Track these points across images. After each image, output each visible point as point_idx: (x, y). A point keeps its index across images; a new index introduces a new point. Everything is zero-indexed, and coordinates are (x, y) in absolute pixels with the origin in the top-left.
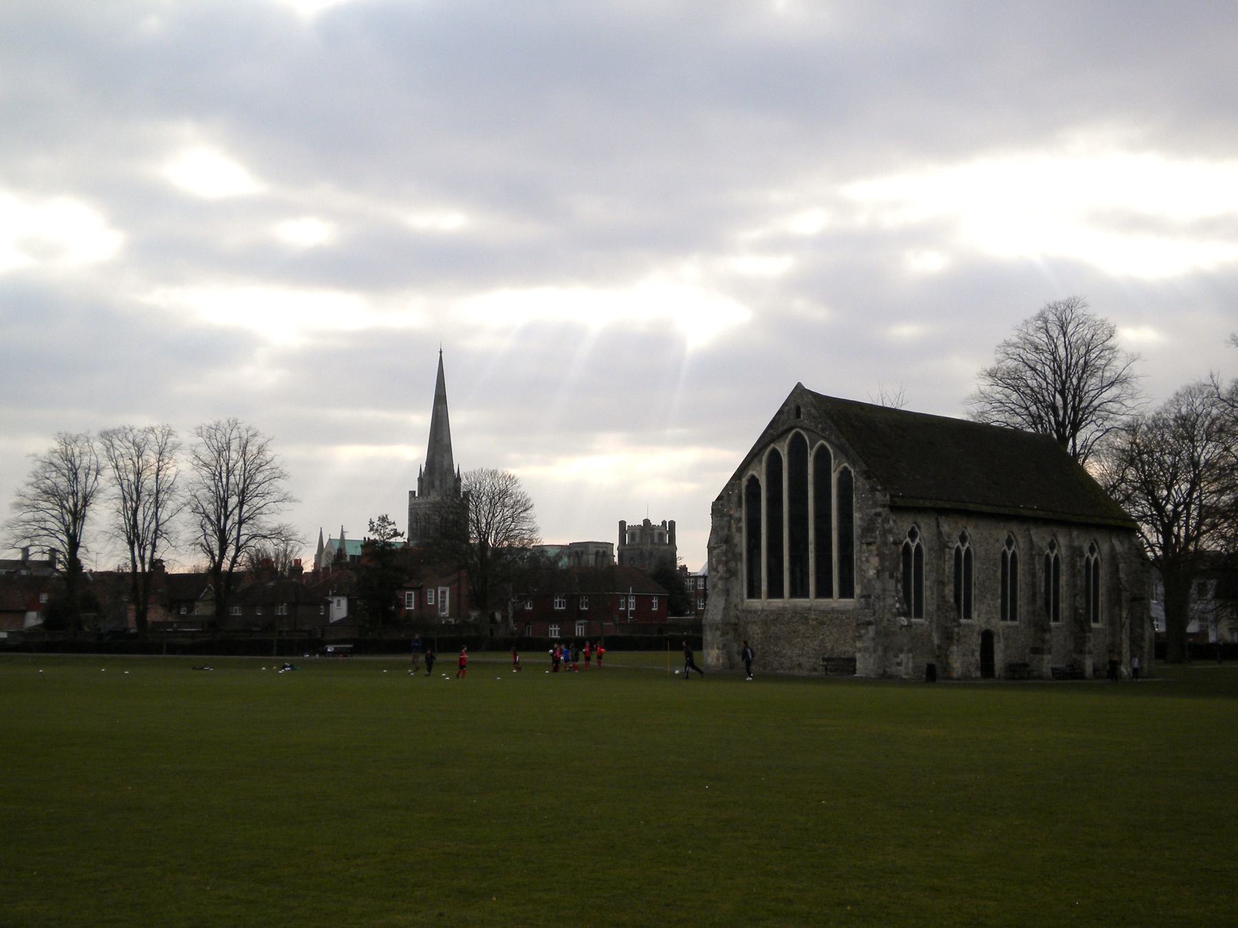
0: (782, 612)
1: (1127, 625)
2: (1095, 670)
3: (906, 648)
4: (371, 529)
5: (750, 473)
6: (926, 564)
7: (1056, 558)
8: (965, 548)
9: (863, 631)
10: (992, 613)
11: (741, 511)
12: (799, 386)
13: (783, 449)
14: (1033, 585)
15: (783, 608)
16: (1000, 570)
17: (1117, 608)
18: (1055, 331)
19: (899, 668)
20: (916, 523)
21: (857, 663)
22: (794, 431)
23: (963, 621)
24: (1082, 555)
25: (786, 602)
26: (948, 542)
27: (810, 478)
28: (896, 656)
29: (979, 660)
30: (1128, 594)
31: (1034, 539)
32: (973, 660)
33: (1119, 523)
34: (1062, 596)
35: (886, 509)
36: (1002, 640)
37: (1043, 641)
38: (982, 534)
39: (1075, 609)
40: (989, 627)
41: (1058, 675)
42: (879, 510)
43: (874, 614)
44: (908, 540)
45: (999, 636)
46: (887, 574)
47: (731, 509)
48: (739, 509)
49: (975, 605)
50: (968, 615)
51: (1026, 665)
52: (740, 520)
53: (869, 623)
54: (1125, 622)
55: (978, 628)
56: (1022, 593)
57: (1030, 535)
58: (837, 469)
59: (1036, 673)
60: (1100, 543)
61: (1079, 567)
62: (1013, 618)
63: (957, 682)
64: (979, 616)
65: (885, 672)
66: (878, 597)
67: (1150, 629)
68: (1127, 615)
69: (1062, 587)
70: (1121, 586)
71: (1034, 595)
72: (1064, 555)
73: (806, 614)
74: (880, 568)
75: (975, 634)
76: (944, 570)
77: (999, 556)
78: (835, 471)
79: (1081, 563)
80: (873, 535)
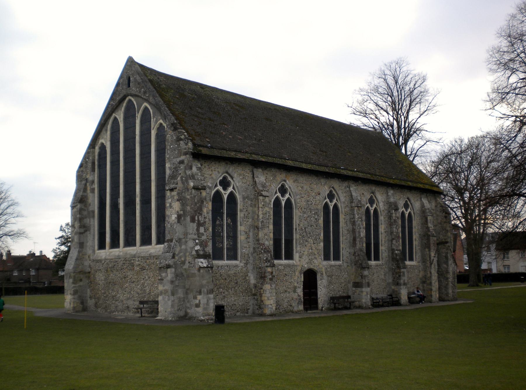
0: (117, 260)
1: (435, 262)
2: (409, 298)
3: (205, 290)
4: (61, 230)
6: (241, 211)
7: (376, 210)
9: (164, 275)
10: (315, 255)
11: (94, 174)
12: (131, 62)
13: (120, 115)
15: (119, 256)
16: (322, 218)
17: (427, 250)
18: (391, 82)
19: (197, 309)
20: (227, 173)
21: (159, 305)
22: (127, 99)
24: (397, 209)
25: (122, 251)
28: (195, 298)
29: (302, 295)
30: (435, 239)
31: (354, 194)
32: (295, 296)
33: (427, 187)
34: (382, 240)
37: (362, 277)
38: (302, 187)
40: (312, 267)
41: (376, 303)
42: (183, 158)
43: (173, 257)
46: (188, 219)
47: (87, 174)
48: (92, 173)
49: (296, 248)
50: (289, 256)
51: (349, 297)
52: (93, 182)
53: (168, 266)
54: (433, 260)
55: (299, 268)
57: (350, 191)
58: (154, 126)
59: (357, 304)
60: (412, 201)
61: (394, 218)
62: (337, 257)
63: (270, 319)
64: (300, 257)
65: (186, 314)
66: (179, 241)
67: (453, 265)
68: (435, 254)
69: (382, 234)
70: (429, 233)
71: (354, 239)
73: (132, 261)
74: (182, 212)
75: (297, 273)
76: (258, 216)
77: (321, 207)
79: (396, 215)
80: (175, 181)
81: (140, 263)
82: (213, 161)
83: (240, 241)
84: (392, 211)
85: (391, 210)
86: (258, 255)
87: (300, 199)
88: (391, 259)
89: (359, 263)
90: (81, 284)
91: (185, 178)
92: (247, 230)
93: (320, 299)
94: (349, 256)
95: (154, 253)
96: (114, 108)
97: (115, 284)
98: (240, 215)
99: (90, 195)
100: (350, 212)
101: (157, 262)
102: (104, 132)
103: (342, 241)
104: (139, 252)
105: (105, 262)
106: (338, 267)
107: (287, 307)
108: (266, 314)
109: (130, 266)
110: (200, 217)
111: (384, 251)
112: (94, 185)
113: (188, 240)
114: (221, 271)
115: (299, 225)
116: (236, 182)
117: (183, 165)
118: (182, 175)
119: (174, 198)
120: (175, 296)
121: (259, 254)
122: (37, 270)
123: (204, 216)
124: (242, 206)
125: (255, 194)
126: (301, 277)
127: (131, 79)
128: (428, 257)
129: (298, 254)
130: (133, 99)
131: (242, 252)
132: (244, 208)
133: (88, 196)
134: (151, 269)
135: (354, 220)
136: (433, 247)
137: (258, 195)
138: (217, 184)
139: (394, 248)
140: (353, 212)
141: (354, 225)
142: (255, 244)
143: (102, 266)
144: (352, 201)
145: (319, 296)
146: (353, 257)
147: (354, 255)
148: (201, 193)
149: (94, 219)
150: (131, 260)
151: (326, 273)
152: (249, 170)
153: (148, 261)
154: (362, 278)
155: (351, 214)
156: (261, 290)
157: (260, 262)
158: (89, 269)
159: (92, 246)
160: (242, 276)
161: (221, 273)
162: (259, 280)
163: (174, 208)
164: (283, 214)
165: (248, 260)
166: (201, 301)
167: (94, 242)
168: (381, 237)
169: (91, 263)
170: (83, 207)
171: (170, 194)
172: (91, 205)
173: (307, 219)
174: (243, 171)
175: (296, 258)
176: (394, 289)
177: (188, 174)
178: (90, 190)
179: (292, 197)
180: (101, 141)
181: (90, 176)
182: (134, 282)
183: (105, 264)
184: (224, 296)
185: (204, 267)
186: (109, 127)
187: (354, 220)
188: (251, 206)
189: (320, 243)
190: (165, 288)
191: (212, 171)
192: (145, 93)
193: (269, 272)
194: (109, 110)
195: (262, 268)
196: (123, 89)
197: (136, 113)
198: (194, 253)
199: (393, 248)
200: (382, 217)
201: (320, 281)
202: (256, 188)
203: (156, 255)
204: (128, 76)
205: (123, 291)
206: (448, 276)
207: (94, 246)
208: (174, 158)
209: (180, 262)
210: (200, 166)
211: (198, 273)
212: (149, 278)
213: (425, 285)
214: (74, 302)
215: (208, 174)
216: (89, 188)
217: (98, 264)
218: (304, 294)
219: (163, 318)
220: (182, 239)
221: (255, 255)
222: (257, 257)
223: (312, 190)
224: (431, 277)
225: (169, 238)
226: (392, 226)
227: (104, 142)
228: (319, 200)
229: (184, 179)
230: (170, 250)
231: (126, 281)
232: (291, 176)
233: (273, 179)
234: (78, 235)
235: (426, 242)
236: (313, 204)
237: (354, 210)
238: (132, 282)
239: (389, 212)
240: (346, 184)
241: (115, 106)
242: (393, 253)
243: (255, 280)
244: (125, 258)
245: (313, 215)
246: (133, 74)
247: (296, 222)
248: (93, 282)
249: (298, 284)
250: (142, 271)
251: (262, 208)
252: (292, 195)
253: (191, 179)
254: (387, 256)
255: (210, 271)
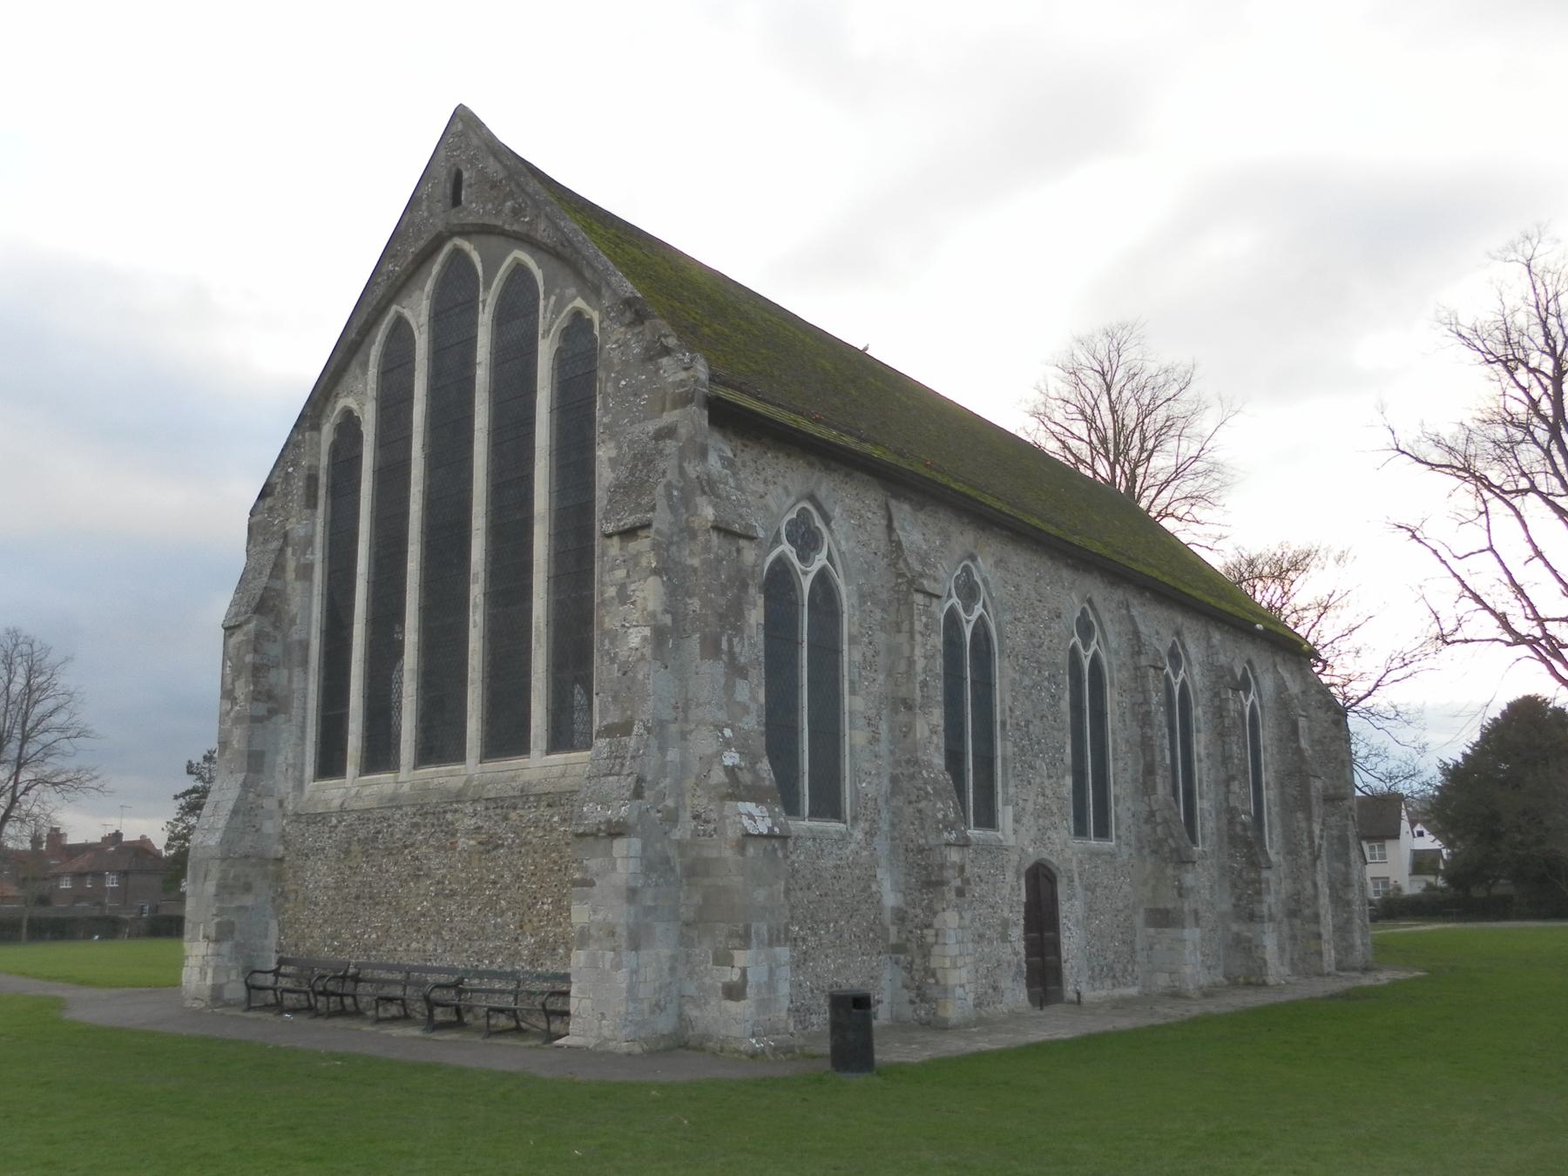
0: (388, 813)
5: (343, 403)
6: (853, 640)
8: (974, 618)
9: (593, 864)
10: (1053, 814)
13: (417, 310)
14: (1146, 744)
17: (1300, 815)
19: (732, 1006)
20: (812, 498)
23: (973, 833)
26: (921, 575)
27: (482, 375)
28: (724, 959)
29: (1023, 952)
31: (1142, 628)
35: (693, 408)
36: (1079, 890)
37: (1182, 892)
38: (1017, 587)
39: (1232, 813)
40: (1045, 855)
44: (786, 548)
45: (1071, 880)
46: (694, 643)
49: (1005, 785)
50: (987, 818)
52: (309, 542)
53: (616, 831)
54: (1320, 845)
56: (1121, 764)
58: (551, 326)
60: (1258, 671)
62: (1102, 831)
64: (1017, 820)
69: (1200, 761)
71: (1149, 770)
72: (1199, 685)
73: (449, 816)
75: (1010, 876)
76: (911, 662)
77: (1063, 658)
78: (547, 332)
80: (645, 500)
81: (480, 824)
82: (769, 449)
83: (851, 750)
84: (1227, 693)
85: (1222, 691)
86: (910, 802)
87: (1011, 623)
88: (1226, 839)
89: (1166, 849)
90: (248, 900)
91: (681, 490)
92: (872, 713)
93: (1068, 965)
94: (1134, 824)
95: (539, 782)
96: (398, 283)
97: (377, 904)
98: (850, 656)
99: (294, 587)
100: (1133, 685)
101: (552, 816)
102: (358, 371)
103: (1114, 775)
104: (475, 783)
105: (340, 822)
106: (1107, 858)
107: (986, 993)
108: (946, 1020)
109: (441, 835)
110: (736, 640)
111: (1207, 815)
112: (312, 553)
113: (693, 726)
114: (793, 857)
115: (1011, 710)
116: (838, 536)
117: (674, 443)
118: (669, 476)
119: (636, 564)
120: (642, 952)
121: (914, 798)
122: (124, 874)
123: (750, 637)
124: (857, 623)
125: (898, 585)
126: (1020, 889)
127: (466, 175)
128: (1305, 838)
129: (1010, 809)
130: (467, 246)
131: (857, 792)
132: (864, 631)
133: (289, 590)
134: (525, 844)
135: (1145, 708)
136: (1317, 810)
137: (908, 589)
138: (778, 533)
139: (1237, 805)
140: (1143, 686)
141: (1145, 724)
142: (897, 763)
143: (329, 838)
144: (1137, 649)
145: (1064, 955)
146: (1147, 828)
147: (1147, 821)
148: (739, 551)
149: (306, 672)
150: (445, 812)
151: (1080, 875)
152: (876, 500)
153: (513, 815)
154: (1180, 895)
155: (1136, 689)
156: (925, 931)
157: (923, 829)
158: (281, 848)
159: (294, 766)
160: (859, 878)
161: (793, 862)
162: (917, 894)
163: (639, 601)
164: (968, 669)
165: (874, 821)
166: (749, 977)
167: (303, 753)
168: (1200, 770)
169: (288, 824)
170: (269, 629)
171: (621, 549)
172: (298, 621)
173: (1031, 694)
174: (857, 500)
175: (1004, 822)
176: (1238, 934)
177: (694, 476)
178: (297, 570)
179: (991, 615)
180: (345, 402)
181: (298, 523)
182: (453, 893)
183: (341, 828)
184: (805, 953)
185: (761, 836)
186: (375, 352)
187: (1145, 708)
188: (883, 629)
189: (1063, 777)
190: (600, 917)
191: (765, 482)
192: (517, 213)
193: (954, 865)
194: (379, 291)
195: (930, 849)
196: (431, 215)
197: (481, 289)
198: (718, 776)
199: (1231, 805)
200: (1200, 709)
201: (1068, 905)
202: (901, 564)
203: (550, 788)
204: (454, 169)
205: (411, 930)
206: (1351, 896)
207: (303, 764)
208: (632, 423)
209: (659, 815)
210: (730, 455)
211: (740, 858)
212: (519, 877)
213: (1297, 922)
214: (216, 969)
215: (753, 493)
216: (291, 565)
217: (313, 828)
218: (1027, 948)
219: (591, 1042)
220: (667, 721)
221: (898, 801)
222: (909, 810)
223: (1040, 601)
224: (1316, 897)
225: (616, 721)
226: (1227, 739)
227: (354, 406)
228: (1059, 636)
229: (675, 493)
230: (622, 765)
231: (422, 892)
232: (990, 546)
233: (942, 546)
234: (245, 726)
235: (1295, 793)
236: (1045, 648)
237: (1145, 677)
238: (447, 896)
239: (1217, 694)
240: (1119, 594)
241: (403, 278)
242: (1231, 822)
243: (900, 896)
244: (422, 806)
245: (1046, 683)
246: (472, 161)
247: (1002, 700)
248: (292, 896)
249: (1011, 912)
250: (488, 852)
251: (922, 635)
252: (990, 609)
253: (704, 493)
254: (1214, 831)
255: (780, 854)
